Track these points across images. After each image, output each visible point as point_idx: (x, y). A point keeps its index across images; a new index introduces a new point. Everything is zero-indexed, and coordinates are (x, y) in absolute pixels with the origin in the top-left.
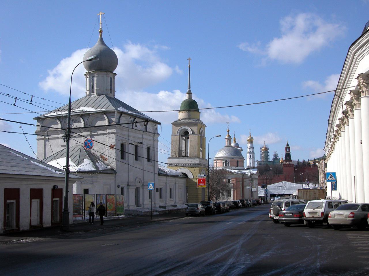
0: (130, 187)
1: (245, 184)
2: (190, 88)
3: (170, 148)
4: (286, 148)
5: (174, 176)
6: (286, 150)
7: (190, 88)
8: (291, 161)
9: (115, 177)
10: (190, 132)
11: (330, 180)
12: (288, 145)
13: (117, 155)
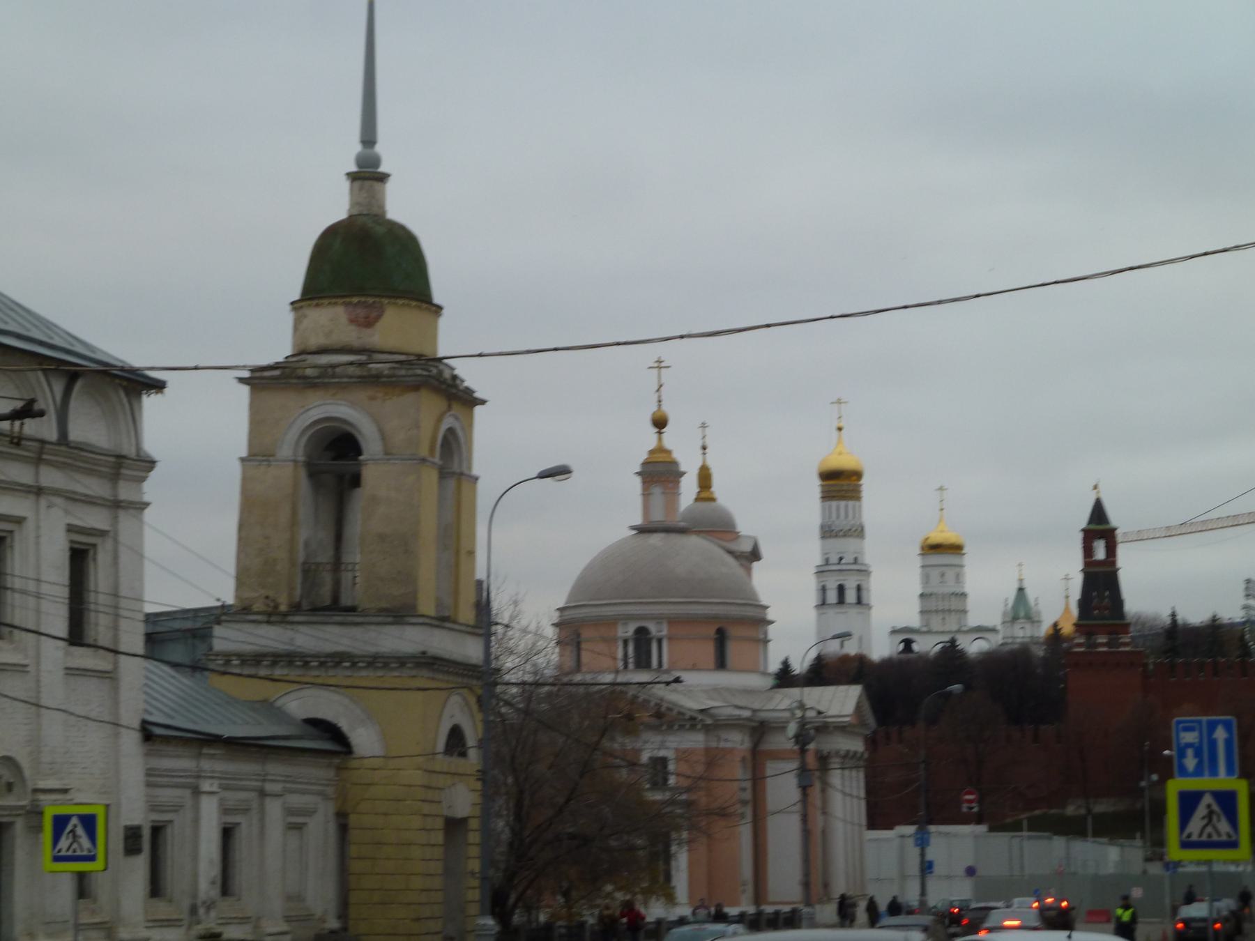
0: (268, 800)
1: (862, 784)
2: (369, 139)
3: (147, 564)
4: (1089, 537)
5: (237, 744)
6: (1088, 550)
7: (369, 139)
8: (1125, 628)
9: (133, 729)
10: (371, 444)
11: (70, 853)
12: (1098, 513)
13: (140, 577)
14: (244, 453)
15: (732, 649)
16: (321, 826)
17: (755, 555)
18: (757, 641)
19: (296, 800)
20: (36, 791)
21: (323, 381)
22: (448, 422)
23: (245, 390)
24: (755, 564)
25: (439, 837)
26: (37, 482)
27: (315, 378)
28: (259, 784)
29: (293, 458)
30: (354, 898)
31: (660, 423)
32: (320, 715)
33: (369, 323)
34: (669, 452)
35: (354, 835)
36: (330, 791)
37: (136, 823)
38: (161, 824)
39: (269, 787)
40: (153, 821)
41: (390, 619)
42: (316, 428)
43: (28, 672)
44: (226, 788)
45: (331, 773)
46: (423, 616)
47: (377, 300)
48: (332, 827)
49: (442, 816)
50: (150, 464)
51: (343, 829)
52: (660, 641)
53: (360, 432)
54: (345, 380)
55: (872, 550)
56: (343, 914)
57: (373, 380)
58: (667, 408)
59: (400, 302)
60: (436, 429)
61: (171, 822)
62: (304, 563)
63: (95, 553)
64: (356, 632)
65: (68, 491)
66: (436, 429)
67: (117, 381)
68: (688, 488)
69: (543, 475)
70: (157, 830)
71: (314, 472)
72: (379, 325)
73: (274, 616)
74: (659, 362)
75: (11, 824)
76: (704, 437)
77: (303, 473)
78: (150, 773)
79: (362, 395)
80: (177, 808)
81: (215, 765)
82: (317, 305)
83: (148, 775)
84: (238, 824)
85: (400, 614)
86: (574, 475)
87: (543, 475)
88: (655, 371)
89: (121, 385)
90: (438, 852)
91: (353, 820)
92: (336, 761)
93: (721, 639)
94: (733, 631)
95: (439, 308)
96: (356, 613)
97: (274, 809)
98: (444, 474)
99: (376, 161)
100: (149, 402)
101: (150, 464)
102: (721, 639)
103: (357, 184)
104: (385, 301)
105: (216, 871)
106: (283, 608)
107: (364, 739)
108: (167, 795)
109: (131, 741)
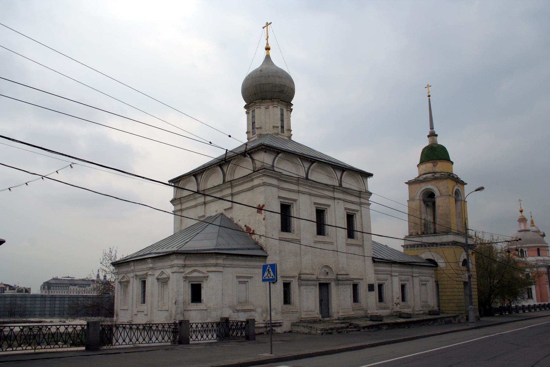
0: (414, 278)
2: (432, 128)
7: (432, 128)
10: (437, 193)
14: (408, 199)
15: (541, 252)
16: (431, 284)
17: (544, 235)
18: (546, 250)
19: (423, 278)
20: (337, 275)
21: (425, 181)
22: (456, 187)
23: (407, 185)
24: (544, 237)
25: (463, 286)
26: (334, 196)
27: (422, 180)
28: (412, 274)
29: (419, 199)
30: (441, 301)
31: (521, 211)
32: (427, 258)
33: (435, 166)
34: (524, 216)
35: (440, 286)
36: (433, 276)
37: (372, 283)
38: (289, 282)
39: (414, 275)
40: (378, 283)
41: (445, 234)
42: (424, 192)
43: (334, 244)
44: (399, 275)
45: (433, 272)
46: (453, 232)
47: (436, 161)
48: (434, 285)
49: (462, 281)
50: (371, 194)
51: (437, 285)
52: (525, 251)
53: (434, 191)
54: (429, 179)
56: (439, 306)
57: (436, 179)
59: (441, 161)
61: (385, 283)
62: (424, 223)
63: (356, 216)
64: (437, 237)
65: (343, 199)
66: (453, 189)
67: (357, 172)
68: (529, 222)
69: (477, 190)
70: (380, 286)
71: (425, 202)
72: (437, 167)
73: (418, 235)
75: (330, 283)
77: (422, 202)
78: (375, 271)
79: (434, 182)
80: (386, 280)
81: (396, 269)
82: (422, 164)
83: (375, 271)
84: (406, 284)
85: (447, 233)
86: (485, 189)
87: (477, 190)
89: (359, 174)
90: (462, 290)
91: (439, 283)
92: (434, 268)
93: (538, 250)
94: (541, 249)
95: (452, 163)
96: (282, 200)
97: (416, 280)
98: (456, 201)
99: (434, 132)
100: (369, 180)
101: (371, 194)
102: (538, 250)
103: (430, 138)
104: (438, 161)
105: (400, 295)
106: (420, 234)
107: (441, 263)
108: (382, 276)
109: (369, 261)
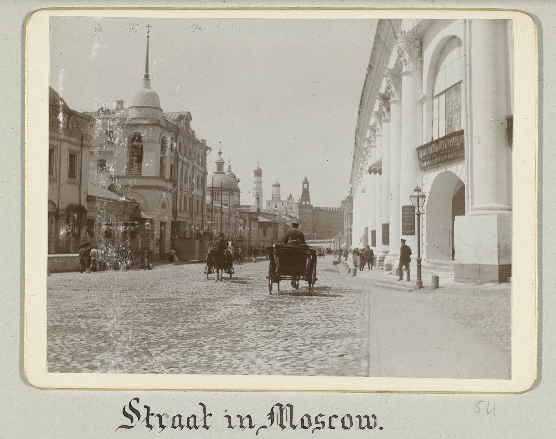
2: (147, 71)
4: (304, 183)
6: (303, 186)
7: (147, 71)
12: (306, 179)
17: (239, 181)
55: (263, 186)
58: (222, 150)
60: (160, 137)
74: (148, 25)
76: (148, 32)
88: (147, 28)
